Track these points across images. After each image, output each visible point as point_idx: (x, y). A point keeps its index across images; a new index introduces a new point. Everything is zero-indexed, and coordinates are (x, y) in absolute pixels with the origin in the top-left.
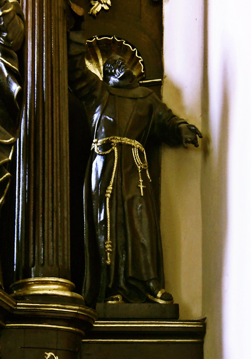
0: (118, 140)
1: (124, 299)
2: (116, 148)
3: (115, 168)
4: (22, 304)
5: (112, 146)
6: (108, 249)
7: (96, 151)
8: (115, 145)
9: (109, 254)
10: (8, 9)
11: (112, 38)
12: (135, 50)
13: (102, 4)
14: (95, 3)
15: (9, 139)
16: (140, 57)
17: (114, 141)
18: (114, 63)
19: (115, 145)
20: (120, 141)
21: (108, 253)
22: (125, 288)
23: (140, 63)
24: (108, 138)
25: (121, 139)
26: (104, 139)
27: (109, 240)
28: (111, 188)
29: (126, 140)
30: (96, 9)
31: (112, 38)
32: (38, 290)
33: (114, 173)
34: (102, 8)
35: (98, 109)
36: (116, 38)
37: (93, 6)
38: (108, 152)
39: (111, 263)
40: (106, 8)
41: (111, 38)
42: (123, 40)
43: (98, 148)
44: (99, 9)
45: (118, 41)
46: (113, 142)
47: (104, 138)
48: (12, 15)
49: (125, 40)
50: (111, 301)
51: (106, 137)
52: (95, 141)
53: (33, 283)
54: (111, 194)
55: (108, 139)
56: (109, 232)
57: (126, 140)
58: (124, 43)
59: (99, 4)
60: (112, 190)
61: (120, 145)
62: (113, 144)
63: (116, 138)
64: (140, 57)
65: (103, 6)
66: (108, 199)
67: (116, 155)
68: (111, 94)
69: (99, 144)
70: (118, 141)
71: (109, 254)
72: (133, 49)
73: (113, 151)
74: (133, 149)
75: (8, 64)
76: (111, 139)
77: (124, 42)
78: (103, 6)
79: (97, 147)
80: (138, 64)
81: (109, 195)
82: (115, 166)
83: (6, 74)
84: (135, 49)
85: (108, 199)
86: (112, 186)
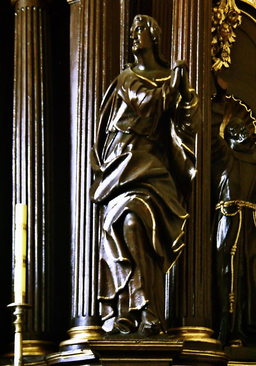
0: (242, 203)
1: (243, 343)
2: (241, 212)
3: (239, 230)
4: (187, 350)
5: (237, 210)
6: (232, 300)
7: (222, 211)
8: (240, 209)
9: (231, 304)
10: (195, 102)
11: (230, 96)
12: (250, 111)
13: (223, 61)
14: (217, 60)
15: (185, 215)
16: (254, 118)
17: (240, 205)
18: (237, 127)
19: (240, 209)
20: (244, 205)
21: (231, 303)
22: (241, 333)
23: (254, 124)
24: (233, 201)
25: (245, 203)
26: (231, 202)
27: (232, 292)
28: (236, 247)
29: (249, 204)
30: (218, 67)
31: (230, 96)
32: (192, 337)
33: (238, 234)
34: (223, 65)
35: (224, 173)
36: (234, 97)
37: (215, 62)
38: (233, 215)
39: (233, 312)
40: (227, 65)
41: (229, 96)
42: (239, 100)
43: (224, 209)
44: (219, 66)
45: (235, 101)
46: (239, 206)
47: (230, 200)
48: (196, 108)
49: (241, 100)
50: (235, 344)
51: (231, 200)
52: (222, 203)
53: (187, 331)
54: (235, 253)
55: (234, 202)
56: (232, 285)
57: (249, 204)
58: (240, 103)
59: (220, 61)
60: (236, 249)
61: (244, 209)
62: (239, 208)
63: (241, 202)
64: (254, 118)
65: (223, 64)
66: (232, 256)
67: (241, 217)
68: (235, 158)
69: (225, 206)
70: (242, 205)
71: (231, 304)
72: (248, 109)
73: (238, 214)
74: (253, 212)
75: (188, 150)
76: (237, 203)
77: (241, 102)
78: (224, 63)
79: (223, 208)
80: (250, 124)
81: (234, 253)
82: (240, 228)
83: (185, 157)
84: (250, 110)
85: (232, 256)
86: (236, 245)
